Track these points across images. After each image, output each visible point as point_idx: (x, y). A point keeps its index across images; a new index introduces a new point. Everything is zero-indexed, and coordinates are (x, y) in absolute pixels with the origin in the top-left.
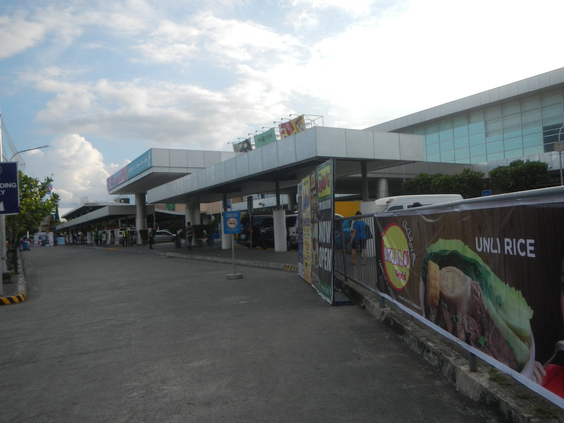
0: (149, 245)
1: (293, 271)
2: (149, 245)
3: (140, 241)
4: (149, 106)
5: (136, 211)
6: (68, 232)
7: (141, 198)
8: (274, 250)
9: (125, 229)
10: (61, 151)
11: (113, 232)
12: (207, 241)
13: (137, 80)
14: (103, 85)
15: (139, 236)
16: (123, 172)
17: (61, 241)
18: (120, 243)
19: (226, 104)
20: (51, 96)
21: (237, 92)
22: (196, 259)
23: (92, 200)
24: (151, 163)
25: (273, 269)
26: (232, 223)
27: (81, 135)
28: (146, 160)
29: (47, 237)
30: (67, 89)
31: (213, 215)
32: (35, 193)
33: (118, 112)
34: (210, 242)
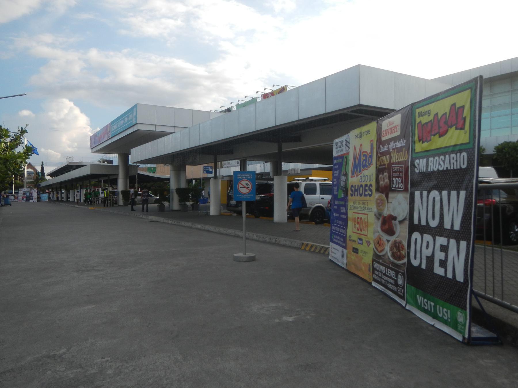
0: (130, 206)
1: (314, 252)
2: (130, 206)
3: (121, 202)
4: (136, 76)
5: (118, 171)
6: (53, 189)
7: (124, 157)
8: (273, 220)
9: (107, 189)
10: (51, 114)
12: (192, 205)
13: (125, 51)
14: (94, 54)
15: (121, 196)
16: (106, 129)
17: (45, 197)
19: (207, 78)
20: (44, 61)
21: (218, 66)
22: (183, 226)
23: (76, 160)
24: (136, 120)
25: (284, 246)
26: (244, 187)
27: (70, 100)
28: (131, 116)
29: (31, 193)
30: (59, 56)
31: (194, 179)
32: (5, 143)
33: (107, 80)
34: (195, 207)
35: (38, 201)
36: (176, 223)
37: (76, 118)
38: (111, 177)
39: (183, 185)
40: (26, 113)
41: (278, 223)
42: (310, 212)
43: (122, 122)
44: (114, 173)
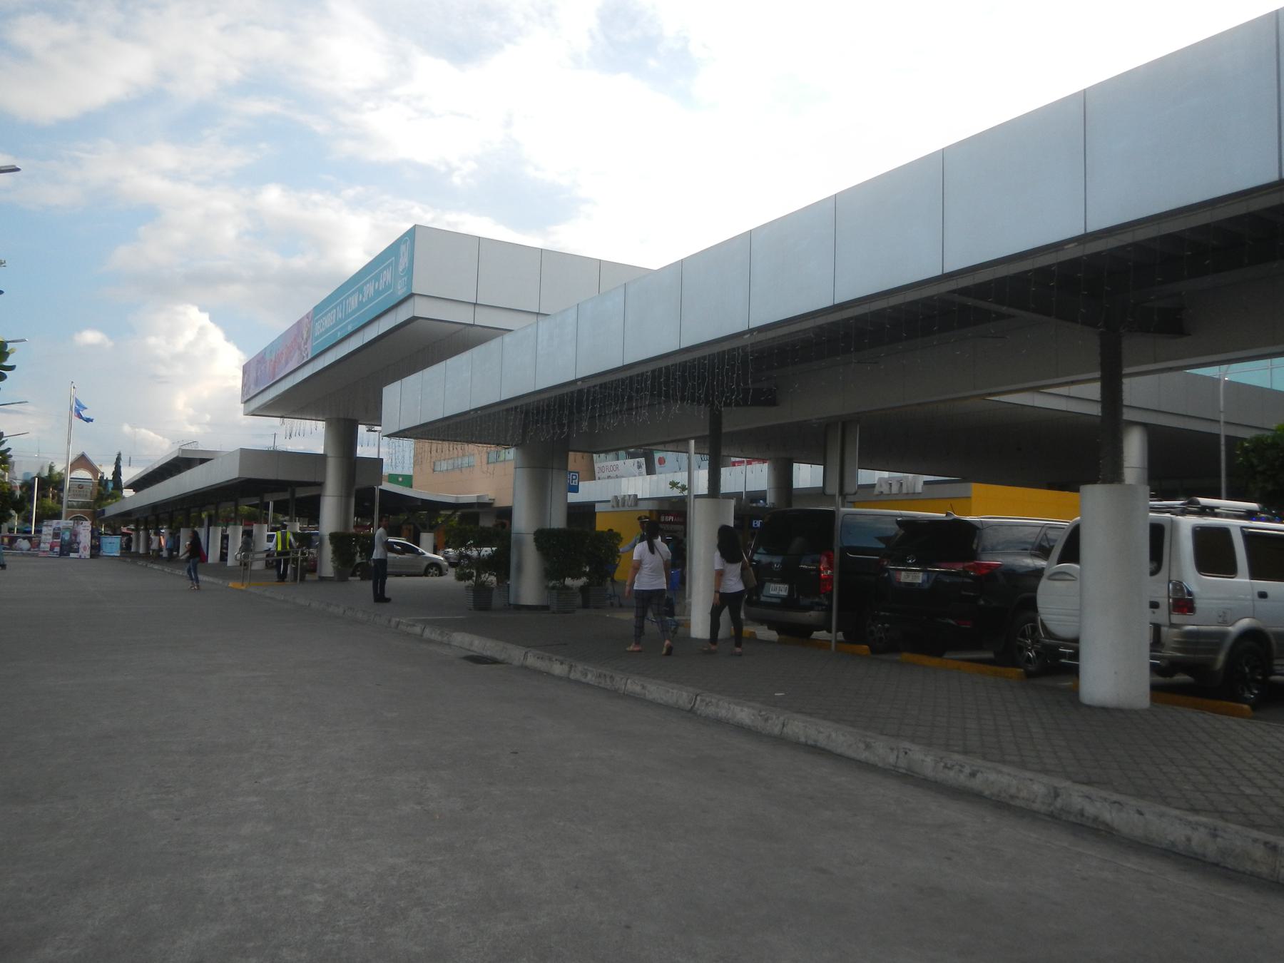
3: (328, 567)
6: (137, 523)
10: (152, 340)
11: (248, 534)
12: (583, 589)
13: (350, 193)
14: (273, 197)
15: (328, 549)
18: (268, 565)
23: (205, 445)
28: (387, 276)
29: (75, 534)
33: (298, 263)
35: (92, 556)
36: (590, 678)
37: (212, 352)
38: (301, 493)
39: (558, 520)
40: (91, 337)
41: (1105, 709)
42: (1221, 658)
43: (354, 302)
44: (312, 480)
